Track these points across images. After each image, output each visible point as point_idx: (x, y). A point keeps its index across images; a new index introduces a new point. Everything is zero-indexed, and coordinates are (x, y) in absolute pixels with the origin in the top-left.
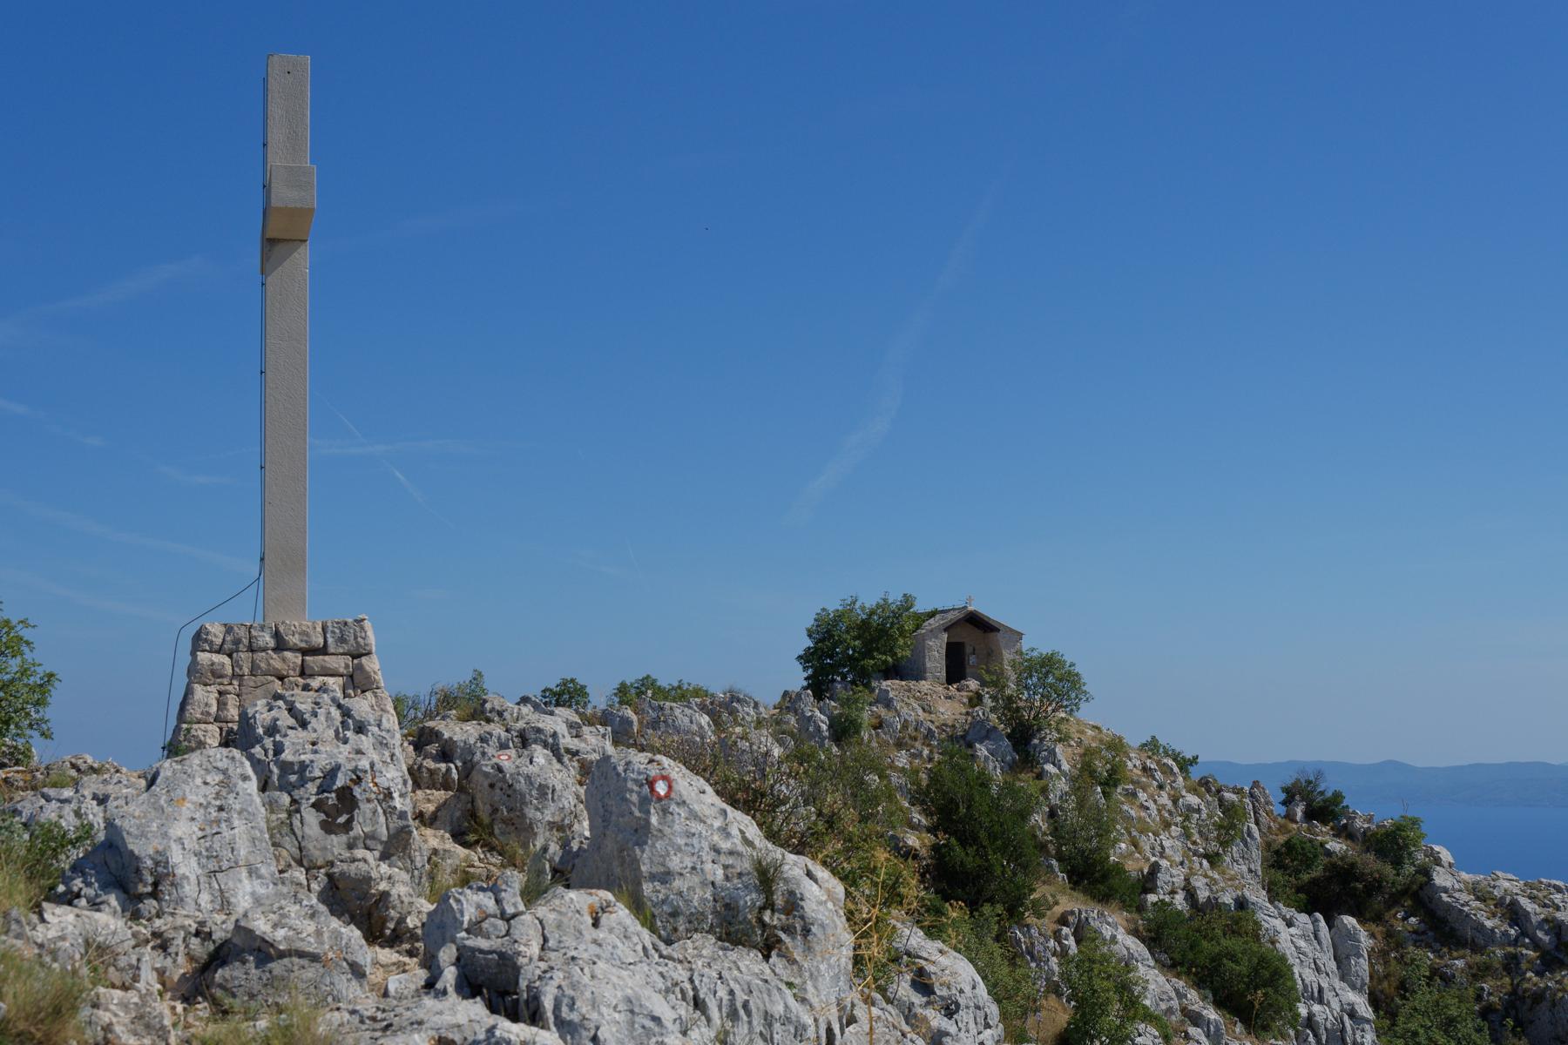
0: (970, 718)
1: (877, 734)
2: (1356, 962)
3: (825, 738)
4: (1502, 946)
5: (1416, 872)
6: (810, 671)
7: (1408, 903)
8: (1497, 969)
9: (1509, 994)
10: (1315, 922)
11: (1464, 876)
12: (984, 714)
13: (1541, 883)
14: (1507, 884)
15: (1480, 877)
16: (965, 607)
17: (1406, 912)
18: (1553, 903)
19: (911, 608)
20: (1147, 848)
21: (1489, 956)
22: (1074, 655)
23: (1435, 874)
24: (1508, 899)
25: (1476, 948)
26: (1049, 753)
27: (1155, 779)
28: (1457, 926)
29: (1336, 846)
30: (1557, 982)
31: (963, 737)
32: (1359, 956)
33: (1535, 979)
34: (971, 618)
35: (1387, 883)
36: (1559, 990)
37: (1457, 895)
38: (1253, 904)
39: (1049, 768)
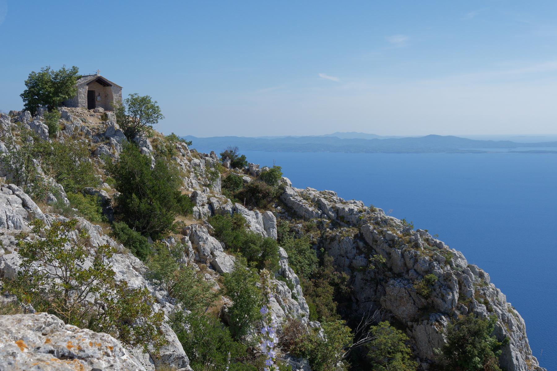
0: (105, 125)
1: (63, 133)
2: (272, 230)
3: (47, 136)
4: (316, 218)
5: (279, 188)
6: (27, 102)
7: (277, 201)
8: (315, 228)
9: (321, 238)
10: (257, 214)
11: (296, 189)
12: (111, 124)
13: (326, 192)
14: (314, 193)
15: (302, 190)
16: (96, 75)
17: (276, 205)
18: (333, 200)
19: (76, 73)
20: (186, 184)
21: (311, 222)
22: (155, 98)
23: (286, 189)
24: (316, 199)
25: (306, 219)
26: (144, 142)
27: (181, 152)
28: (297, 210)
29: (248, 178)
30: (340, 232)
31: (104, 134)
32: (274, 228)
33: (330, 231)
34: (99, 79)
35: (271, 193)
36: (341, 236)
37: (296, 197)
38: (240, 210)
39: (144, 149)
